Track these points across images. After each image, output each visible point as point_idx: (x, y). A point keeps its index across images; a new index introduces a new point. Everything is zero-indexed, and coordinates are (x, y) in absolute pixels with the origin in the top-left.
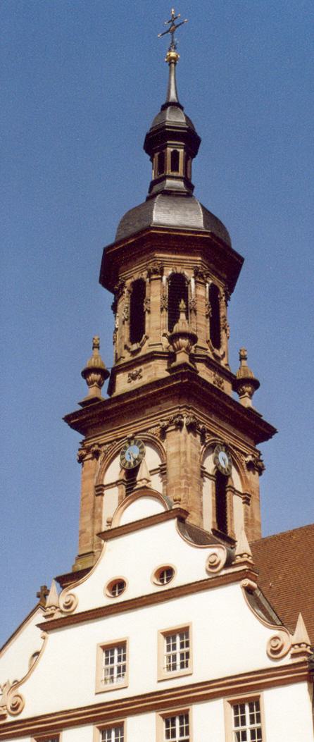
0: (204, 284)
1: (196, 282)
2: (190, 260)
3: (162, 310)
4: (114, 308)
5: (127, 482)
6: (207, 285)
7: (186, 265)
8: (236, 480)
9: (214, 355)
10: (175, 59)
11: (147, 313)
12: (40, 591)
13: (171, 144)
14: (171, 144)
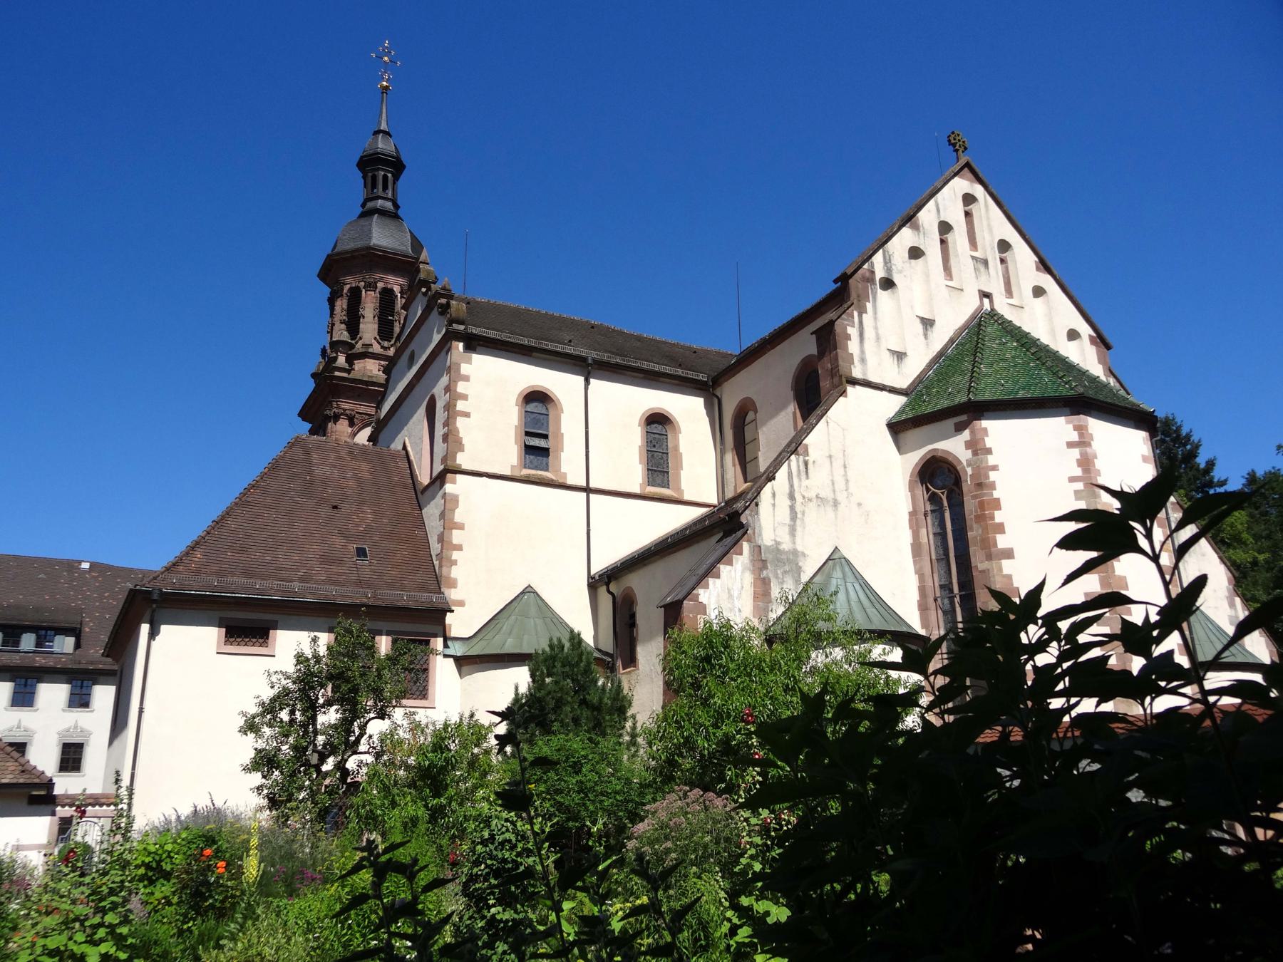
7: (396, 283)
9: (382, 347)
13: (379, 169)
14: (379, 169)
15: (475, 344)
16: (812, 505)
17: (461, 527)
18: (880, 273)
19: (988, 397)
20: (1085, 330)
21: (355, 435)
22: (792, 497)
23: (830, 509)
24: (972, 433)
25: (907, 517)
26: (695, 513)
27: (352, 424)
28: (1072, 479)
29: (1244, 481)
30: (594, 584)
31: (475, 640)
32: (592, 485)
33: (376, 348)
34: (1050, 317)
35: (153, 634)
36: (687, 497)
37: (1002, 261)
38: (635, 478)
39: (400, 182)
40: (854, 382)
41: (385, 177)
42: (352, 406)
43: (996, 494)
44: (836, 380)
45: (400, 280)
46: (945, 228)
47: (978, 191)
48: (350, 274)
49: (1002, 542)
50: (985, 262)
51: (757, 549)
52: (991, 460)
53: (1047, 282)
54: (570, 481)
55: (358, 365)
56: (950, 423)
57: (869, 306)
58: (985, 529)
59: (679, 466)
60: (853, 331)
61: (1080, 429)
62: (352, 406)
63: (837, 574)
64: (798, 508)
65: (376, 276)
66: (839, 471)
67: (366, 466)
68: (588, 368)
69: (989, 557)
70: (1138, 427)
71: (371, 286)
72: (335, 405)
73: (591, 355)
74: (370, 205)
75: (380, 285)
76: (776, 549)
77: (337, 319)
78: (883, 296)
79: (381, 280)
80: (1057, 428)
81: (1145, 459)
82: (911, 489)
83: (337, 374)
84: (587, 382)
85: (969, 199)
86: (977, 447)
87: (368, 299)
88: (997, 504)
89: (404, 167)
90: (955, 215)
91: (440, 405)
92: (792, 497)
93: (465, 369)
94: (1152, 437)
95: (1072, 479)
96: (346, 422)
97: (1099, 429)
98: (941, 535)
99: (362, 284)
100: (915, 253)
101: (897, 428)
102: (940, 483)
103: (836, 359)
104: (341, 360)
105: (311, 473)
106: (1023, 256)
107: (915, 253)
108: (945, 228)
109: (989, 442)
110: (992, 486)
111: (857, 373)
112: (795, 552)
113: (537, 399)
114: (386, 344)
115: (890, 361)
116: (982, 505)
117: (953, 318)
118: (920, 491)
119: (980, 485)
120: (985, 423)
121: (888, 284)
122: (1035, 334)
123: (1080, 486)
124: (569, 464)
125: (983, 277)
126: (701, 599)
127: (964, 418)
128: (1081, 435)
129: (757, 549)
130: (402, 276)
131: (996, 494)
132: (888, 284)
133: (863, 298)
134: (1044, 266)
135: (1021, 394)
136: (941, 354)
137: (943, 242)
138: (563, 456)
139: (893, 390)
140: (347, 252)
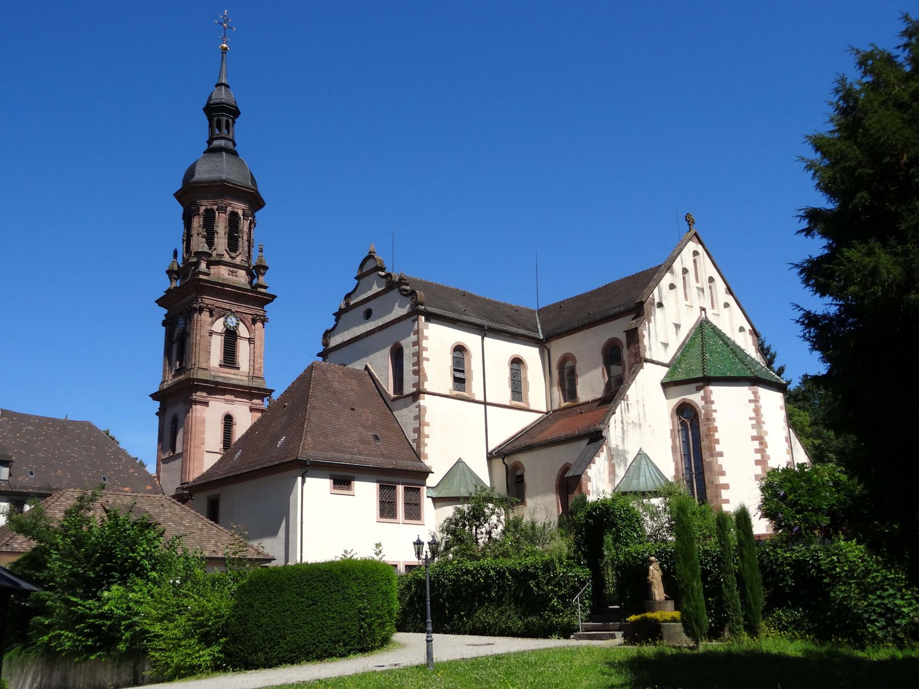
7: (240, 207)
8: (243, 331)
13: (220, 115)
14: (220, 115)
15: (431, 317)
16: (631, 426)
17: (428, 425)
18: (657, 300)
19: (712, 374)
20: (747, 327)
21: (213, 323)
22: (622, 423)
23: (638, 428)
24: (705, 392)
25: (669, 432)
26: (535, 417)
27: (211, 315)
28: (751, 419)
29: (800, 380)
30: (491, 457)
31: (441, 487)
32: (488, 400)
33: (226, 258)
34: (731, 319)
35: (303, 482)
36: (532, 408)
37: (710, 288)
38: (506, 399)
40: (647, 361)
41: (227, 122)
43: (716, 424)
44: (638, 359)
45: (242, 206)
46: (685, 271)
47: (700, 248)
48: (205, 198)
49: (718, 448)
50: (703, 290)
51: (609, 449)
52: (714, 407)
53: (730, 300)
54: (477, 398)
55: (214, 270)
56: (694, 386)
57: (652, 318)
58: (710, 442)
59: (527, 390)
60: (645, 333)
61: (755, 393)
63: (644, 462)
64: (625, 428)
65: (227, 202)
66: (641, 408)
67: (354, 382)
68: (483, 331)
69: (712, 456)
70: (778, 391)
71: (222, 209)
73: (486, 323)
74: (216, 143)
75: (229, 209)
76: (617, 449)
77: (194, 232)
78: (658, 311)
80: (743, 392)
81: (781, 408)
82: (672, 418)
83: (201, 277)
84: (483, 339)
85: (696, 253)
86: (707, 399)
87: (221, 220)
88: (716, 429)
90: (690, 266)
91: (408, 352)
92: (622, 423)
93: (426, 332)
94: (785, 395)
95: (751, 419)
96: (208, 314)
97: (762, 392)
98: (686, 442)
99: (215, 207)
100: (672, 287)
101: (665, 385)
102: (686, 415)
103: (639, 348)
104: (203, 266)
105: (331, 387)
106: (720, 285)
107: (672, 287)
108: (685, 271)
109: (713, 398)
110: (714, 420)
111: (648, 356)
112: (624, 451)
113: (460, 349)
114: (233, 255)
115: (661, 347)
116: (709, 429)
117: (689, 323)
118: (676, 418)
119: (708, 419)
120: (711, 388)
121: (660, 305)
122: (724, 331)
123: (754, 422)
124: (476, 388)
125: (702, 299)
126: (589, 474)
127: (701, 384)
128: (755, 397)
129: (609, 449)
130: (244, 203)
131: (716, 424)
132: (660, 305)
133: (650, 314)
134: (730, 291)
135: (728, 374)
136: (683, 343)
137: (684, 278)
138: (473, 383)
139: (663, 365)
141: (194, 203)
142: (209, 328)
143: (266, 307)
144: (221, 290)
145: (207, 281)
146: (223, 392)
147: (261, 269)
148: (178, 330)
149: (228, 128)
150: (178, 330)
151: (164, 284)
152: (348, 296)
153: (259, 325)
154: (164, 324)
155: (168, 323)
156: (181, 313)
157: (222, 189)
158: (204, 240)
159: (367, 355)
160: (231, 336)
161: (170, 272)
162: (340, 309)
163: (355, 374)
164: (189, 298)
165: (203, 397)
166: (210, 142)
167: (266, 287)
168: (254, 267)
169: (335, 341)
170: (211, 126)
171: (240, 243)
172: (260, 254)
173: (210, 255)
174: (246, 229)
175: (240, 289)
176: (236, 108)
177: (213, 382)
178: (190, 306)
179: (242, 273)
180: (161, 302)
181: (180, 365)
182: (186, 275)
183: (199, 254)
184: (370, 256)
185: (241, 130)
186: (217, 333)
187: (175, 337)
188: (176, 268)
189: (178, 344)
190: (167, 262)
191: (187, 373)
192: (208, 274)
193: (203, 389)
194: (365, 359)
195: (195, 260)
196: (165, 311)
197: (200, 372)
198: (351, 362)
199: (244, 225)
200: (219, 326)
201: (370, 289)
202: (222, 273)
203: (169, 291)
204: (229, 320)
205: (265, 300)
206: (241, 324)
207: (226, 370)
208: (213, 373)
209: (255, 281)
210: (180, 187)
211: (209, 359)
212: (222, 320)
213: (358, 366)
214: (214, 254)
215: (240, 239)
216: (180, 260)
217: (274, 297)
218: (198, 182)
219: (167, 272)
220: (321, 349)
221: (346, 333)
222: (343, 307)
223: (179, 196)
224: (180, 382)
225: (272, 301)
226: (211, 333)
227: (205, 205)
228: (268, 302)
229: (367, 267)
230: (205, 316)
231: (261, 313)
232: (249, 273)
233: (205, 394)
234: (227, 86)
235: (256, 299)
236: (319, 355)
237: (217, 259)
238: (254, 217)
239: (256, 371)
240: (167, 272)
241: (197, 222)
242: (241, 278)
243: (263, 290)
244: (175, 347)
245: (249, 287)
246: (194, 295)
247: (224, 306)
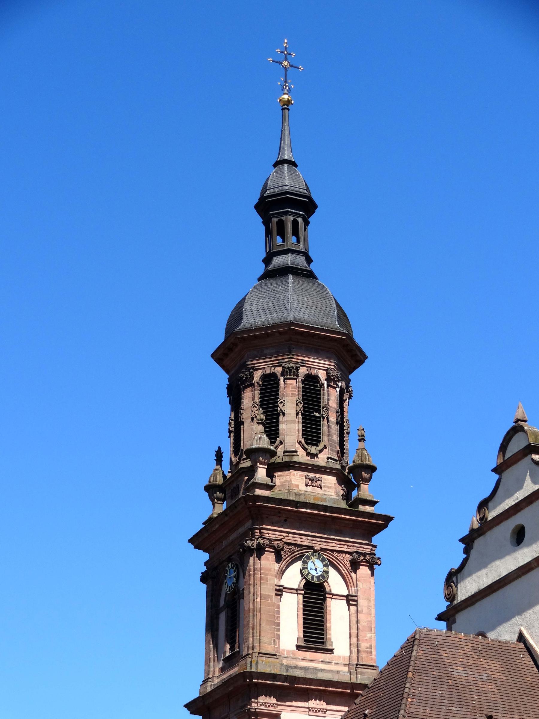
0: (335, 388)
1: (328, 386)
2: (348, 546)
3: (297, 414)
4: (230, 437)
5: (267, 423)
6: (338, 389)
7: (320, 367)
8: (335, 583)
9: (309, 454)
10: (288, 102)
11: (281, 414)
12: (204, 569)
13: (284, 212)
14: (284, 212)
27: (279, 559)
33: (302, 457)
39: (309, 228)
41: (295, 223)
42: (279, 535)
45: (325, 363)
48: (262, 356)
55: (281, 478)
62: (279, 535)
67: (495, 665)
71: (290, 373)
72: (257, 533)
74: (278, 261)
75: (303, 371)
77: (245, 416)
79: (303, 364)
83: (259, 492)
87: (289, 390)
89: (315, 206)
99: (279, 370)
104: (261, 473)
105: (449, 675)
114: (313, 450)
130: (328, 358)
140: (259, 329)
141: (244, 366)
142: (276, 581)
143: (375, 540)
144: (293, 513)
145: (268, 499)
146: (305, 695)
147: (364, 471)
148: (226, 588)
149: (296, 233)
150: (226, 588)
151: (205, 509)
152: (484, 505)
153: (364, 571)
154: (204, 578)
155: (211, 577)
156: (229, 559)
157: (291, 338)
158: (261, 428)
159: (520, 612)
160: (314, 595)
161: (210, 489)
162: (472, 531)
163: (501, 648)
164: (241, 530)
165: (270, 705)
166: (267, 261)
167: (373, 503)
168: (351, 470)
169: (467, 588)
170: (268, 233)
171: (325, 429)
172: (361, 445)
173: (273, 454)
174: (333, 403)
175: (325, 508)
176: (309, 198)
177: (286, 678)
178: (242, 545)
179: (330, 481)
180: (197, 541)
181: (232, 648)
182: (236, 491)
183: (253, 453)
184: (517, 429)
185: (320, 235)
186: (290, 590)
187: (222, 603)
188: (220, 480)
189: (227, 613)
190: (206, 471)
191: (242, 663)
192: (270, 488)
193: (270, 691)
194: (518, 618)
195: (246, 464)
196: (206, 556)
197: (263, 660)
198: (493, 628)
199: (330, 397)
200: (293, 577)
201: (520, 487)
202: (294, 484)
203: (209, 522)
204: (310, 565)
205: (372, 526)
206: (332, 572)
207: (308, 655)
208: (285, 662)
209: (354, 494)
210: (222, 339)
211: (278, 637)
212: (298, 565)
213: (506, 633)
214: (280, 451)
215: (324, 422)
216: (226, 467)
217: (388, 519)
218: (249, 330)
219: (208, 488)
220: (443, 606)
221: (484, 572)
222: (476, 525)
223: (221, 356)
224: (231, 679)
225: (385, 526)
226: (280, 591)
227: (262, 368)
228: (380, 528)
229: (514, 448)
230: (268, 560)
231: (367, 549)
232: (343, 480)
233: (272, 700)
234: (293, 164)
235: (356, 525)
236: (440, 617)
237: (286, 459)
238: (348, 382)
239: (363, 655)
240: (208, 488)
241: (250, 398)
242: (330, 490)
243: (368, 509)
244: (223, 617)
245: (343, 505)
246: (248, 524)
247: (300, 540)
